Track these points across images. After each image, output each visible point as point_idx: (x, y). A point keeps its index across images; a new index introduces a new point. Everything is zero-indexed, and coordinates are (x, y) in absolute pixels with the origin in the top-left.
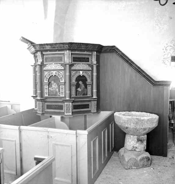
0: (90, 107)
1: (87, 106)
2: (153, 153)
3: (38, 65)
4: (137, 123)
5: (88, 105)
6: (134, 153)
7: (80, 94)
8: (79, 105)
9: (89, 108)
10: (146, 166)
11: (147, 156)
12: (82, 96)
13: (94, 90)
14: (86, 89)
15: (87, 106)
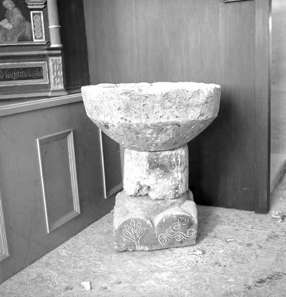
0: (46, 76)
1: (36, 73)
2: (229, 204)
3: (13, 8)
4: (128, 108)
5: (40, 69)
6: (141, 203)
7: (9, 39)
8: (11, 70)
9: (41, 77)
10: (182, 244)
11: (183, 214)
12: (15, 43)
13: (50, 23)
14: (27, 23)
15: (36, 73)
